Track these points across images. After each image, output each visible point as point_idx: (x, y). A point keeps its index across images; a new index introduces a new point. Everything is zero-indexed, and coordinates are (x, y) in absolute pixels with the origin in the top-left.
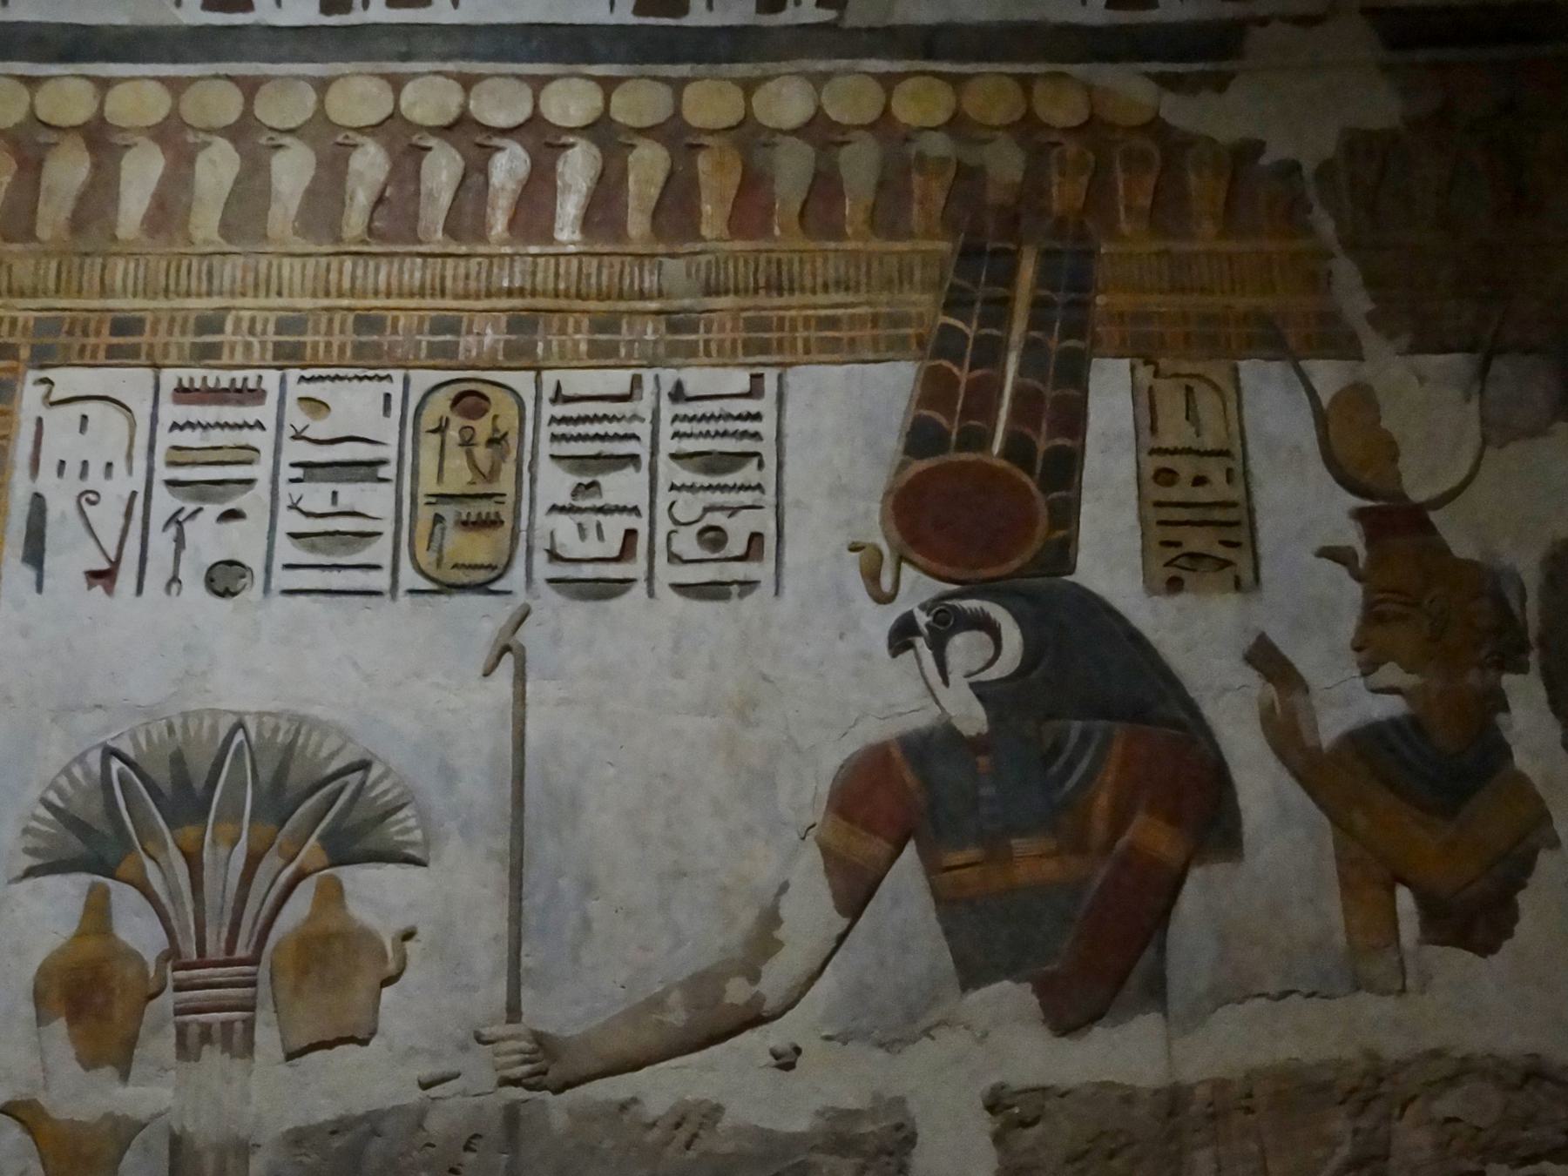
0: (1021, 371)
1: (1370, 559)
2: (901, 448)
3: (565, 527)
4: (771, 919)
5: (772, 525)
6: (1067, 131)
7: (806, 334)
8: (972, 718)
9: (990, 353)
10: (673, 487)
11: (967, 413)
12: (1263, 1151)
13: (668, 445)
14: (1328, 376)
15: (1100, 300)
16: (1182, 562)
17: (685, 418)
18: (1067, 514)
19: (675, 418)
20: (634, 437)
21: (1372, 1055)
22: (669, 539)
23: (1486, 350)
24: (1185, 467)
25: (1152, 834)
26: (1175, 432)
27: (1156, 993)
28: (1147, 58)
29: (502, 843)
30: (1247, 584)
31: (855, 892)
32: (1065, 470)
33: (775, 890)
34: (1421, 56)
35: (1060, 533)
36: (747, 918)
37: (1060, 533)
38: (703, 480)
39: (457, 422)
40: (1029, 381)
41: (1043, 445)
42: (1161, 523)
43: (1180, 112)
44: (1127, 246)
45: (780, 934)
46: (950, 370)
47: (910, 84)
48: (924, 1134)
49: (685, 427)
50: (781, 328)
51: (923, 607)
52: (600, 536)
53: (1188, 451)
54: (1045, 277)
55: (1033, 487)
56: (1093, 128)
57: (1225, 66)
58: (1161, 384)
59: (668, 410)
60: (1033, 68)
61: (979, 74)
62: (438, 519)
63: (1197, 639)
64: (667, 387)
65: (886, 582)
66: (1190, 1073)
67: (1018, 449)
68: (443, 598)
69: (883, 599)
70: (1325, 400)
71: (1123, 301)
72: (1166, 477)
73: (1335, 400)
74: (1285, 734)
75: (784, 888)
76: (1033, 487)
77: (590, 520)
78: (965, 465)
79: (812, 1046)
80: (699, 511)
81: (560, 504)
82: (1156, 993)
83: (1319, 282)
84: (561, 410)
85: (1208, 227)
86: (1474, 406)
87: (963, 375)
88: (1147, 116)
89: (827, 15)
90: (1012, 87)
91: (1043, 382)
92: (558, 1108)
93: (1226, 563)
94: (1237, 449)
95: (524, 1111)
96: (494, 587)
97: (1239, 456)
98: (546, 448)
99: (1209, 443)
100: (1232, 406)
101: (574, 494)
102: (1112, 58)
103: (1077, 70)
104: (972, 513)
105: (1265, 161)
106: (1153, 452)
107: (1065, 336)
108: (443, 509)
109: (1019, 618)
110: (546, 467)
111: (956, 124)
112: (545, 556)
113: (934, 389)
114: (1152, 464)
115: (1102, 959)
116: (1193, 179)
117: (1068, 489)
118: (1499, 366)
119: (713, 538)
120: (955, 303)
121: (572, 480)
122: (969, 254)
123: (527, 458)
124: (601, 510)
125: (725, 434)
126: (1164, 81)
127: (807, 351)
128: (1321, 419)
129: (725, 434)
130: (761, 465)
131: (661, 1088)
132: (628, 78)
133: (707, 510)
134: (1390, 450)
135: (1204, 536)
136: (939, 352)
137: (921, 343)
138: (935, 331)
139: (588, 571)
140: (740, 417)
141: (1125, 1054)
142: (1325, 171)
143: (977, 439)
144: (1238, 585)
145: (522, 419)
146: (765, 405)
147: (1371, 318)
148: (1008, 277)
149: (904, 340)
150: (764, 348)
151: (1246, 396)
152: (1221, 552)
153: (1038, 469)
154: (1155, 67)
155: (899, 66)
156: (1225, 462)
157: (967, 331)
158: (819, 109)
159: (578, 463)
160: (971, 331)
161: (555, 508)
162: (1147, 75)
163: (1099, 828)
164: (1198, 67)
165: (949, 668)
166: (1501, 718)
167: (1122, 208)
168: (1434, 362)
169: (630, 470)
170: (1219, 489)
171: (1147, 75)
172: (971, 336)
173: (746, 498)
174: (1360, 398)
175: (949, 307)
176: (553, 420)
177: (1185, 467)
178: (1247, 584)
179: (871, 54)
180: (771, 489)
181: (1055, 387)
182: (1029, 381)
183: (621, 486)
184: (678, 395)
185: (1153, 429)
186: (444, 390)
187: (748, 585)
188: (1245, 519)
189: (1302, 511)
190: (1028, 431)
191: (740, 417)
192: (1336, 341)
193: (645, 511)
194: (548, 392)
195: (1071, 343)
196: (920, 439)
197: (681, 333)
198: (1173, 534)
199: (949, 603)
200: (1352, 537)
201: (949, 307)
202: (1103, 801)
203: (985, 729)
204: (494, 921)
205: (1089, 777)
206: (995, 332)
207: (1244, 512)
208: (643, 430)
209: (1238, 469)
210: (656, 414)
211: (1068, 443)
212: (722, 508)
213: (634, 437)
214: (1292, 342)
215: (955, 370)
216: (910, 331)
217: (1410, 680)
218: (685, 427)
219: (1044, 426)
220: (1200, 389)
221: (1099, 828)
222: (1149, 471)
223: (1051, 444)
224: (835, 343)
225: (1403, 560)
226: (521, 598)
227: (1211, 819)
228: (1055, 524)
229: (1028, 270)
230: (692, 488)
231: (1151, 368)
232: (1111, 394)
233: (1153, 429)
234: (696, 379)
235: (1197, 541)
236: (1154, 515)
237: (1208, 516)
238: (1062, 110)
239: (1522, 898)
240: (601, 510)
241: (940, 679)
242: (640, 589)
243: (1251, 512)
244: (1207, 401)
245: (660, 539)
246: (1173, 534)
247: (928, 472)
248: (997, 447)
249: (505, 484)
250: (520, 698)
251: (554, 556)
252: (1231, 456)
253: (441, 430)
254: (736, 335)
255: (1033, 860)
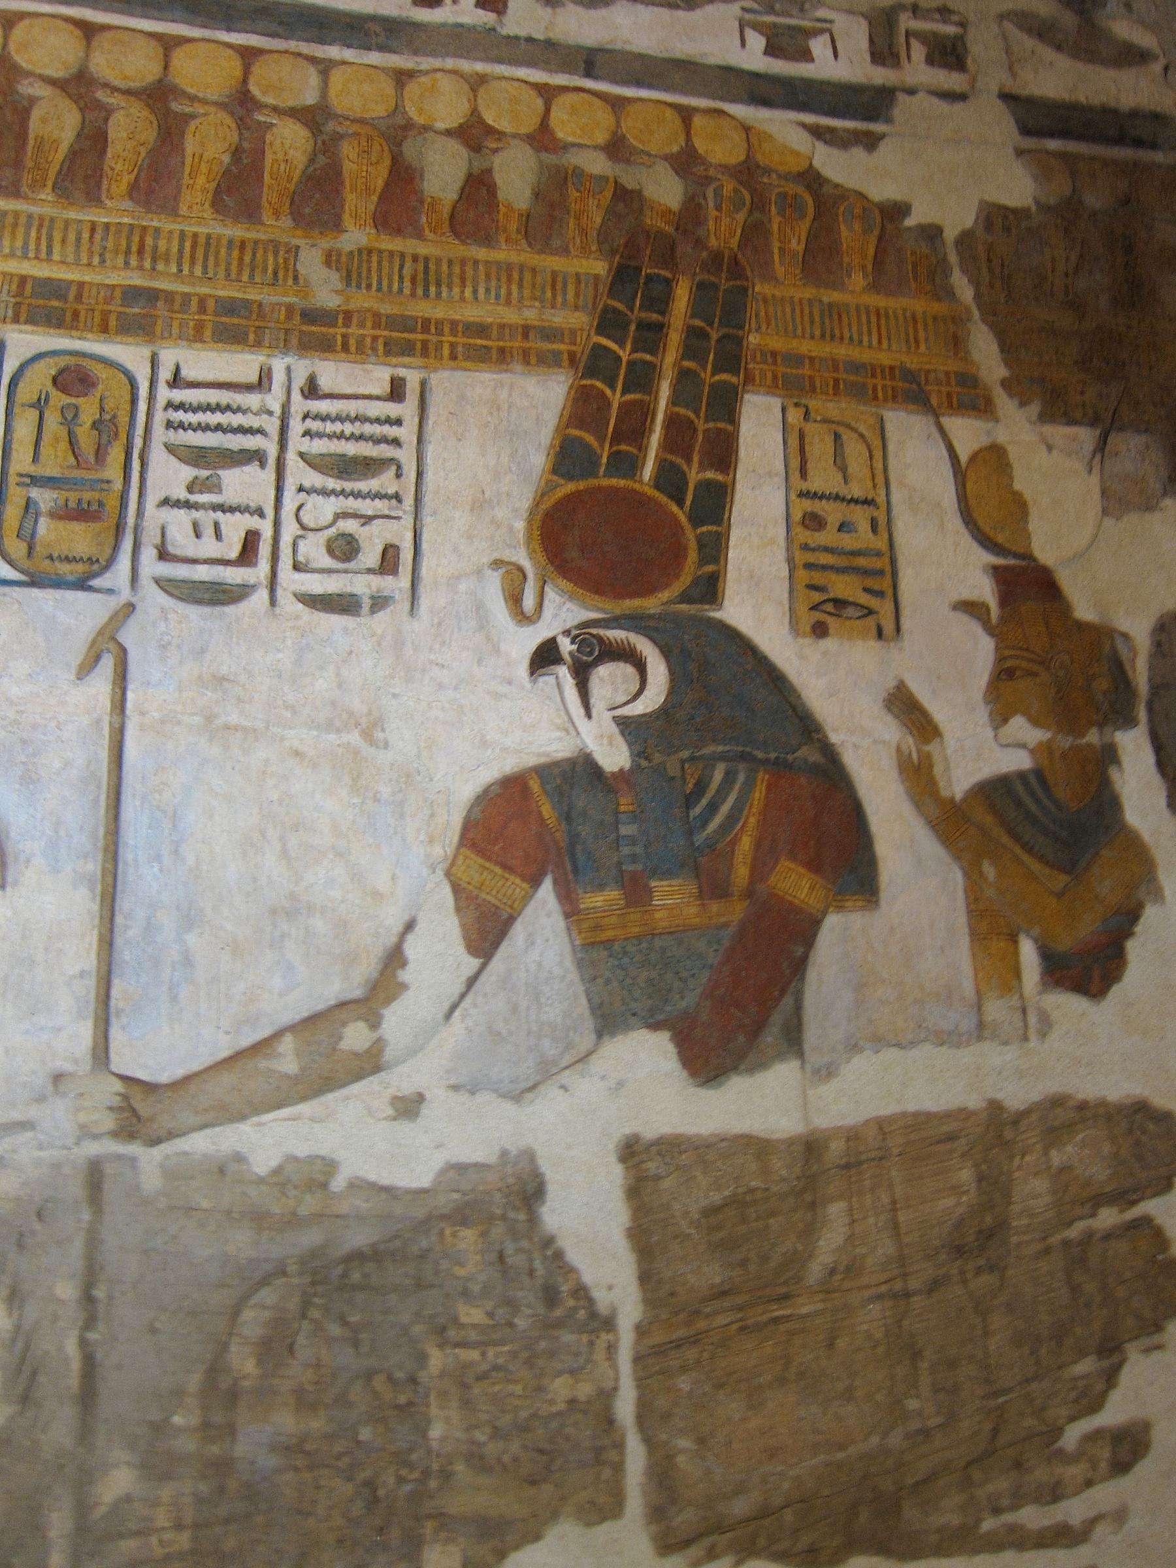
0: (674, 401)
1: (1002, 618)
2: (549, 466)
3: (179, 523)
4: (395, 958)
5: (409, 535)
6: (724, 168)
7: (451, 339)
8: (614, 756)
9: (642, 379)
10: (301, 489)
11: (617, 438)
12: (894, 1202)
13: (297, 443)
14: (967, 433)
15: (754, 339)
16: (829, 607)
17: (318, 417)
18: (714, 550)
19: (306, 416)
20: (260, 431)
21: (995, 1107)
22: (295, 545)
23: (1106, 425)
24: (833, 513)
25: (796, 883)
26: (823, 478)
27: (793, 1040)
28: (803, 107)
29: (93, 867)
30: (888, 632)
31: (487, 931)
32: (714, 505)
33: (400, 928)
34: (1053, 144)
35: (710, 568)
36: (367, 967)
37: (710, 568)
38: (332, 483)
39: (59, 399)
40: (682, 411)
41: (694, 476)
42: (808, 566)
43: (835, 166)
44: (780, 288)
45: (404, 976)
46: (603, 393)
47: (570, 98)
48: (552, 1189)
49: (315, 425)
50: (426, 329)
51: (567, 633)
52: (218, 536)
53: (837, 497)
54: (699, 307)
55: (683, 519)
56: (748, 172)
57: (878, 127)
58: (810, 428)
59: (299, 404)
60: (694, 102)
61: (641, 100)
62: (29, 503)
63: (838, 686)
64: (299, 381)
65: (529, 602)
66: (822, 1122)
67: (670, 480)
68: (35, 592)
69: (523, 618)
70: (964, 457)
71: (776, 343)
72: (814, 522)
73: (973, 459)
74: (918, 775)
75: (410, 926)
76: (683, 519)
77: (206, 518)
78: (615, 490)
79: (437, 1095)
80: (330, 517)
81: (174, 497)
82: (793, 1040)
83: (957, 343)
84: (178, 395)
85: (858, 280)
86: (1095, 479)
87: (616, 398)
88: (804, 165)
89: (486, 17)
90: (673, 121)
91: (697, 413)
92: (150, 1162)
93: (870, 612)
94: (881, 499)
95: (109, 1169)
96: (96, 583)
97: (884, 508)
98: (160, 434)
99: (857, 491)
100: (878, 454)
101: (190, 489)
102: (765, 102)
103: (739, 110)
104: (622, 537)
105: (909, 222)
106: (801, 495)
107: (717, 370)
108: (35, 493)
109: (666, 652)
110: (159, 457)
111: (616, 148)
112: (155, 552)
113: (584, 409)
114: (801, 507)
115: (737, 1005)
116: (844, 232)
117: (720, 525)
118: (1115, 440)
119: (345, 549)
120: (609, 323)
121: (187, 473)
122: (624, 276)
123: (138, 442)
124: (217, 507)
125: (361, 438)
126: (817, 132)
127: (453, 357)
128: (960, 473)
129: (361, 438)
130: (398, 475)
131: (267, 1141)
132: (271, 52)
133: (338, 516)
134: (1019, 507)
135: (849, 587)
136: (591, 371)
137: (572, 357)
138: (587, 352)
139: (202, 573)
140: (378, 421)
141: (764, 1103)
142: (965, 240)
143: (627, 465)
144: (880, 634)
145: (134, 401)
146: (407, 409)
147: (1004, 383)
148: (661, 301)
149: (557, 354)
150: (407, 349)
151: (891, 447)
152: (864, 599)
153: (688, 503)
154: (810, 118)
155: (560, 79)
156: (869, 511)
157: (621, 353)
158: (475, 112)
159: (196, 456)
160: (625, 355)
161: (166, 502)
162: (804, 126)
163: (741, 873)
164: (850, 124)
165: (592, 701)
166: (1114, 773)
167: (776, 251)
168: (1059, 433)
169: (252, 469)
170: (864, 537)
171: (804, 126)
172: (625, 359)
173: (380, 506)
174: (994, 457)
175: (601, 329)
176: (170, 405)
177: (833, 513)
178: (888, 632)
179: (531, 63)
180: (409, 501)
181: (707, 420)
182: (682, 411)
183: (239, 483)
184: (312, 390)
185: (804, 473)
186: (41, 365)
187: (379, 602)
188: (888, 569)
189: (942, 565)
190: (679, 461)
191: (378, 421)
192: (971, 398)
193: (270, 512)
194: (165, 374)
195: (724, 377)
196: (568, 458)
197: (316, 332)
198: (818, 578)
199: (594, 631)
200: (985, 590)
201: (601, 329)
202: (746, 843)
203: (627, 765)
204: (81, 956)
205: (732, 819)
206: (648, 357)
207: (887, 561)
208: (272, 425)
209: (882, 521)
210: (286, 407)
211: (720, 477)
212: (356, 516)
213: (260, 431)
214: (934, 401)
215: (608, 392)
216: (563, 347)
217: (1037, 736)
218: (315, 425)
219: (696, 458)
220: (847, 437)
221: (741, 873)
222: (797, 516)
223: (700, 476)
224: (484, 348)
225: (1042, 638)
226: (126, 594)
227: (846, 858)
228: (703, 561)
229: (682, 295)
230: (326, 493)
231: (802, 411)
232: (761, 425)
233: (804, 473)
234: (332, 373)
235: (844, 587)
236: (800, 557)
237: (851, 563)
238: (722, 150)
239: (1132, 947)
240: (217, 507)
241: (582, 711)
242: (261, 596)
243: (893, 562)
244: (854, 450)
245: (286, 539)
246: (818, 578)
247: (578, 493)
248: (648, 470)
249: (113, 471)
250: (119, 705)
251: (163, 555)
252: (876, 506)
253: (40, 405)
254: (377, 332)
255: (671, 897)
